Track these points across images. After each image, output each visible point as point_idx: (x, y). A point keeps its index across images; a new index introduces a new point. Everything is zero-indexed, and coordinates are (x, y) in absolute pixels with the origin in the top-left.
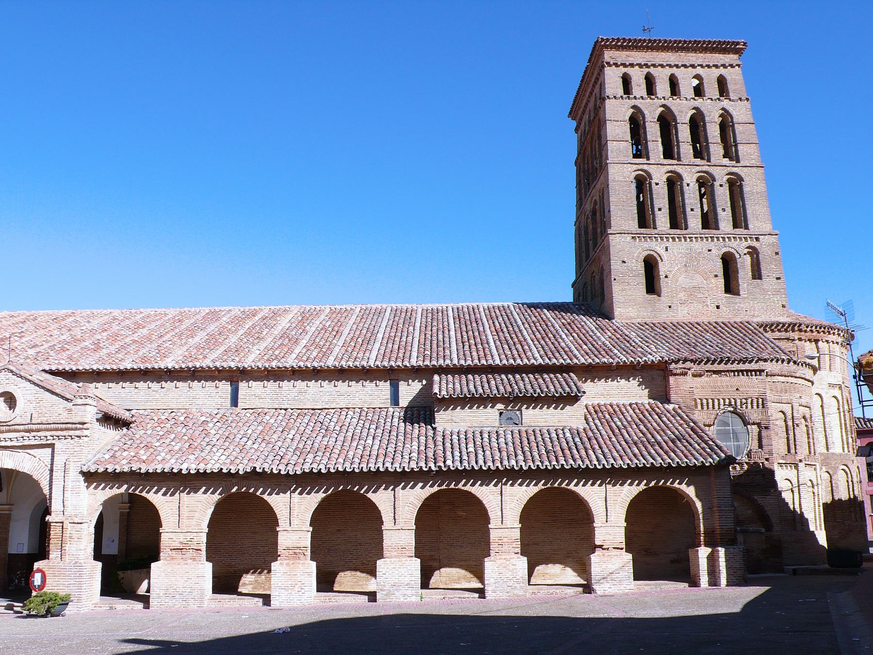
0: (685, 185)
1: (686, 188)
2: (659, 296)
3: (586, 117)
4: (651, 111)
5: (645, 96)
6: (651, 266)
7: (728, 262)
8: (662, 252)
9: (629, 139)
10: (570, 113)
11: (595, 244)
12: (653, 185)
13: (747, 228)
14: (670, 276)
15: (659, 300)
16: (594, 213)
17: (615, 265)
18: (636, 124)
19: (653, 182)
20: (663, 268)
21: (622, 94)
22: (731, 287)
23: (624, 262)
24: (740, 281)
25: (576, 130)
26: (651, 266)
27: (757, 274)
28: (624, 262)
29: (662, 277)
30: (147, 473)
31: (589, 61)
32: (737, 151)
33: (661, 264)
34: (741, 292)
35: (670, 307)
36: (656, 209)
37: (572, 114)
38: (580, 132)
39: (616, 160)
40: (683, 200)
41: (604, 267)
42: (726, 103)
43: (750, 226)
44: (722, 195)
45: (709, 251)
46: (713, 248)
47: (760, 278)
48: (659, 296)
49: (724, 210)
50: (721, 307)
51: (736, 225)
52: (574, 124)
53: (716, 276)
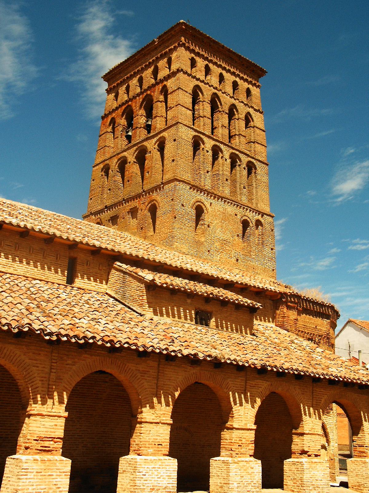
8: (208, 206)
14: (211, 227)
45: (236, 215)
46: (238, 214)
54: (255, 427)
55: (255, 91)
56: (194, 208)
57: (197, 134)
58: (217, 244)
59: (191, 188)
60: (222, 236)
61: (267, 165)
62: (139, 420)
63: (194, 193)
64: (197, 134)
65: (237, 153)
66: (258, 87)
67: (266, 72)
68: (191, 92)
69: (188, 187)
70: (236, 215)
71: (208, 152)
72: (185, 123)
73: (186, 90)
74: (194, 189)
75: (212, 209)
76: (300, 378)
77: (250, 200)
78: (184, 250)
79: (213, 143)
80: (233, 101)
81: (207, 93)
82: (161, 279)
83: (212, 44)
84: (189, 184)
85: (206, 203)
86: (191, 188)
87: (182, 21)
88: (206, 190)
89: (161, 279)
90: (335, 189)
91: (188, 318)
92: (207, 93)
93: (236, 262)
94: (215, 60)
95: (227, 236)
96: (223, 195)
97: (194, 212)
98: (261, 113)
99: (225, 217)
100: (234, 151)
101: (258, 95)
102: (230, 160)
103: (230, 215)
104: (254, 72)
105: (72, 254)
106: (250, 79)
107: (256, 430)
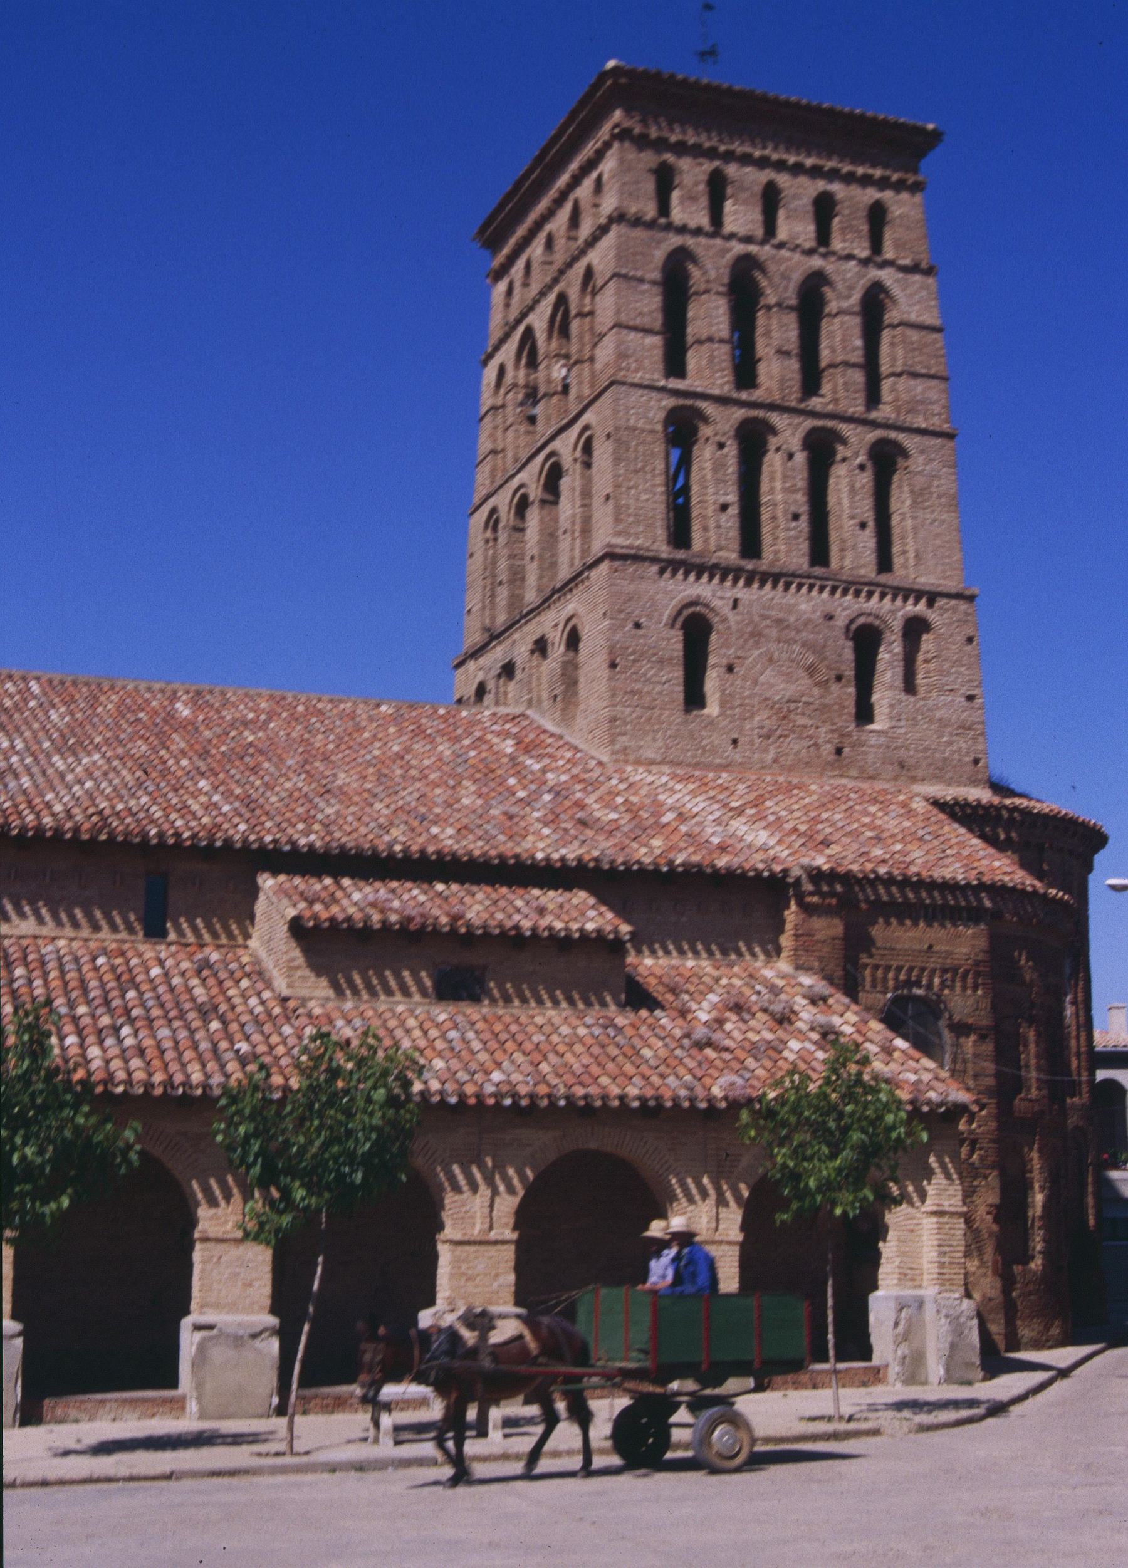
7: (866, 640)
54: (514, 1236)
55: (903, 207)
56: (679, 624)
57: (681, 402)
59: (662, 572)
61: (950, 436)
64: (681, 402)
65: (830, 424)
66: (916, 188)
68: (656, 275)
69: (655, 568)
72: (636, 380)
73: (639, 274)
74: (674, 573)
75: (739, 618)
76: (652, 1113)
77: (885, 562)
78: (650, 754)
80: (816, 262)
81: (712, 265)
82: (356, 899)
84: (654, 560)
85: (716, 603)
86: (662, 572)
87: (611, 64)
88: (716, 566)
89: (356, 899)
91: (414, 989)
92: (712, 265)
93: (832, 757)
94: (740, 148)
96: (776, 570)
98: (929, 272)
100: (820, 423)
101: (916, 214)
102: (805, 454)
104: (898, 149)
106: (878, 173)
107: (518, 1243)
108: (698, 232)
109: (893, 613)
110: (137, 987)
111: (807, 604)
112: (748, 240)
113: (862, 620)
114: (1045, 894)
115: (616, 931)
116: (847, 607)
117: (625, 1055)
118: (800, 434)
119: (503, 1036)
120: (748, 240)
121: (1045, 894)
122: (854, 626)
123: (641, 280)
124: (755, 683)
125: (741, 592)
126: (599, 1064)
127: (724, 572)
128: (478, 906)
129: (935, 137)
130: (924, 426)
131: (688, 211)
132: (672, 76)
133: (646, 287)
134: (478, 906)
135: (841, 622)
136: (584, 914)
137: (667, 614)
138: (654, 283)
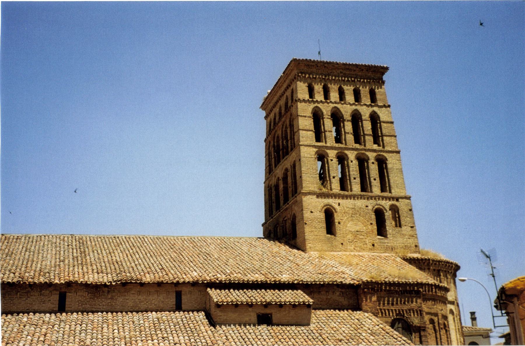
0: (350, 161)
1: (350, 164)
2: (335, 236)
3: (276, 110)
4: (326, 109)
5: (324, 100)
6: (329, 215)
7: (379, 214)
8: (336, 206)
9: (313, 129)
10: (262, 106)
11: (286, 200)
12: (329, 161)
13: (390, 192)
14: (342, 223)
15: (335, 239)
16: (285, 178)
17: (307, 215)
18: (317, 116)
19: (329, 159)
20: (337, 218)
21: (354, 102)
22: (381, 231)
23: (312, 212)
24: (387, 228)
25: (266, 118)
26: (329, 215)
27: (398, 224)
28: (312, 212)
29: (337, 224)
30: (207, 318)
31: (284, 73)
32: (383, 140)
33: (335, 215)
34: (388, 236)
35: (342, 244)
36: (331, 177)
37: (264, 106)
38: (269, 119)
39: (306, 143)
40: (349, 171)
41: (297, 215)
42: (376, 109)
43: (393, 191)
44: (373, 169)
45: (367, 206)
46: (369, 205)
47: (400, 226)
48: (335, 236)
49: (375, 179)
50: (375, 245)
51: (383, 189)
52: (264, 114)
53: (371, 224)
58: (350, 236)
60: (354, 228)
62: (414, 299)
63: (320, 200)
67: (387, 69)
70: (367, 206)
71: (332, 160)
73: (305, 115)
79: (375, 154)
83: (326, 65)
85: (334, 205)
90: (298, 83)
95: (360, 227)
97: (322, 216)
99: (355, 213)
103: (360, 208)
105: (177, 290)
108: (321, 102)
109: (386, 204)
110: (30, 252)
111: (360, 203)
112: (336, 103)
113: (376, 207)
114: (439, 285)
115: (308, 302)
116: (371, 204)
117: (313, 338)
118: (354, 156)
119: (278, 334)
120: (336, 103)
121: (439, 285)
122: (374, 209)
123: (305, 117)
124: (346, 226)
125: (340, 201)
126: (306, 341)
127: (336, 196)
128: (270, 296)
129: (387, 69)
130: (390, 150)
131: (319, 97)
132: (310, 60)
133: (307, 118)
134: (270, 296)
135: (370, 207)
136: (301, 297)
137: (320, 208)
138: (351, 133)
